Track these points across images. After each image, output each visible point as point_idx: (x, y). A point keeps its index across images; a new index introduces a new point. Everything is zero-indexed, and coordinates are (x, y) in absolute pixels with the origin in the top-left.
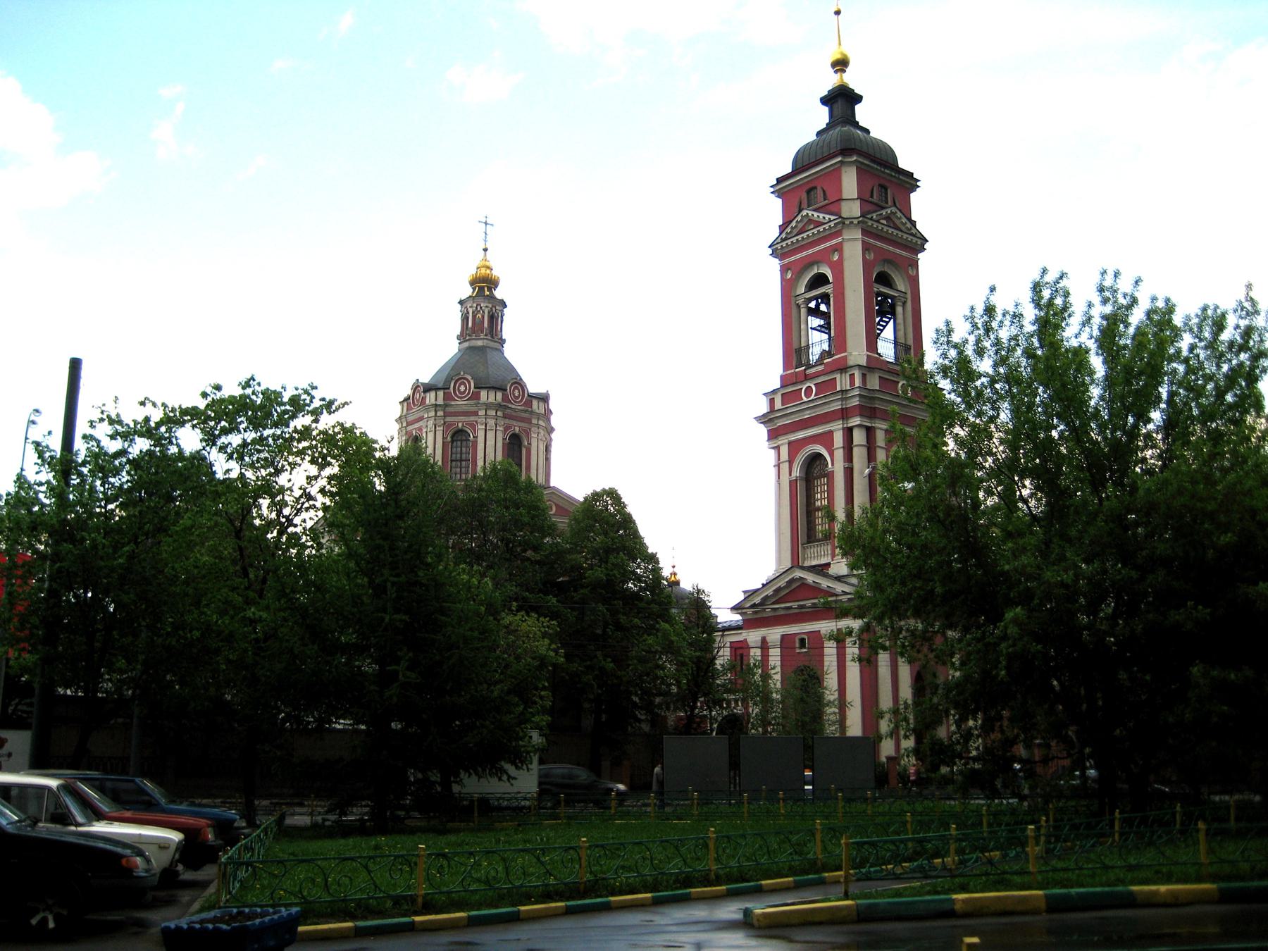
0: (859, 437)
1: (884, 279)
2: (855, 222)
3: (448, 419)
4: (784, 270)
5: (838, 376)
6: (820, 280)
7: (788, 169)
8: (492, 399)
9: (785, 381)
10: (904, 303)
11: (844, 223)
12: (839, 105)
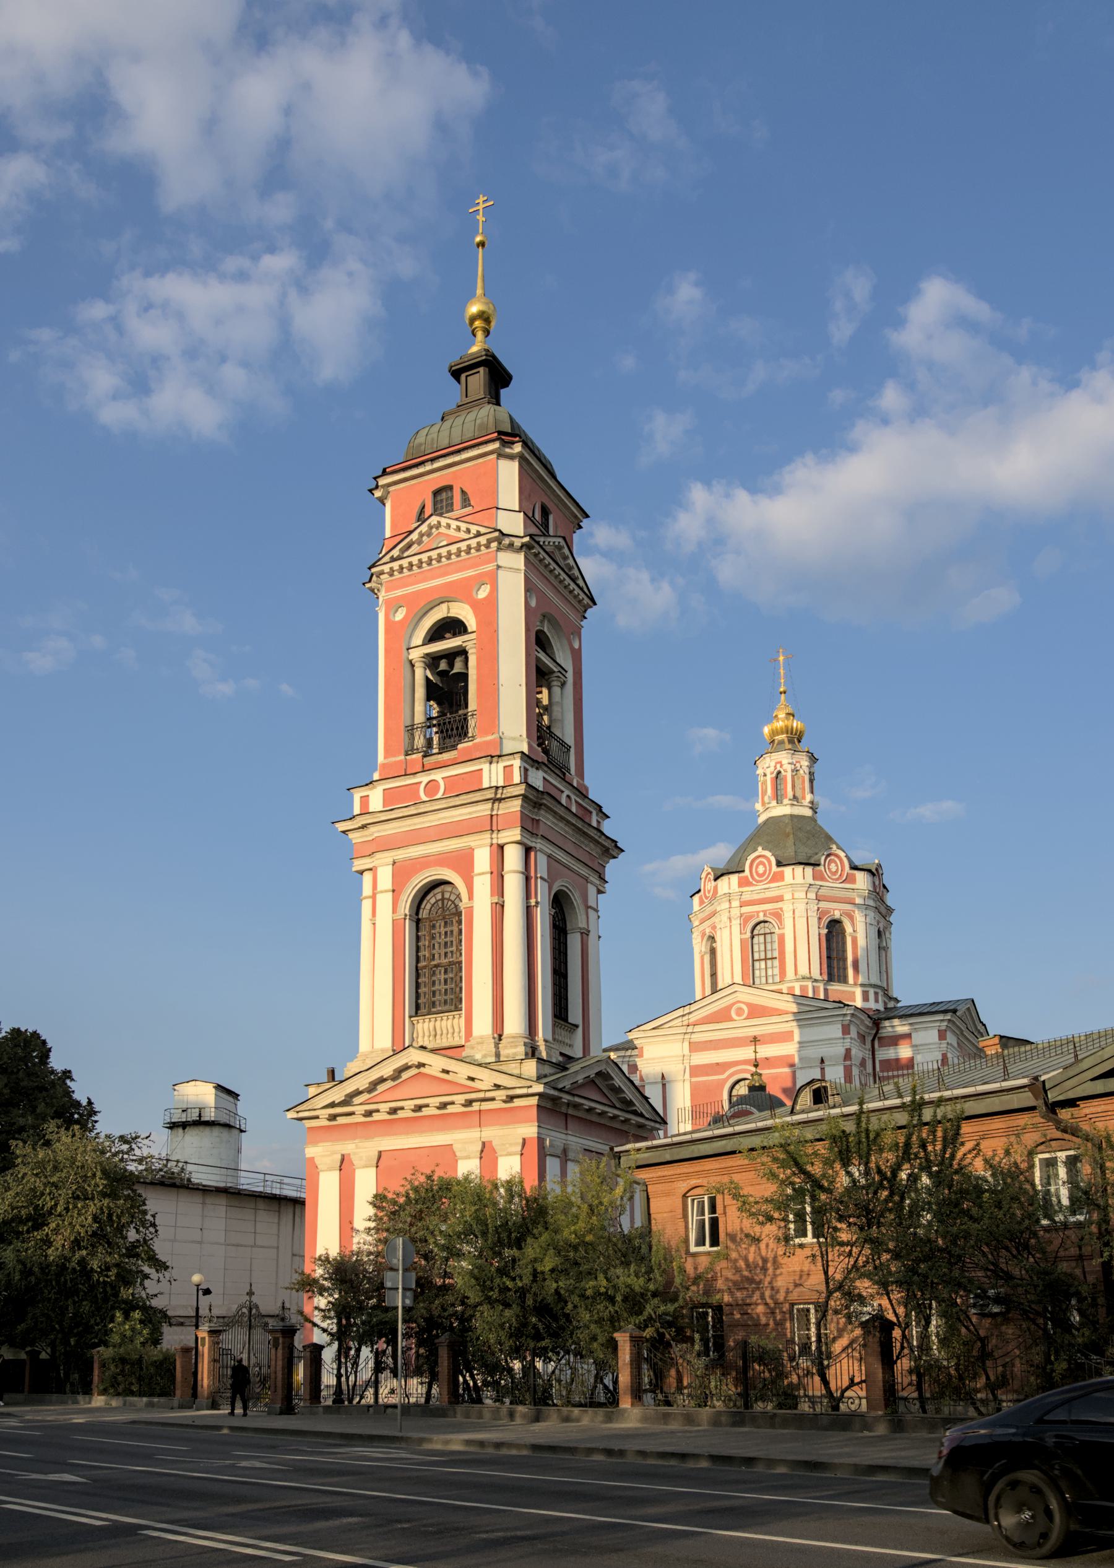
2: (518, 543)
3: (745, 909)
5: (485, 767)
6: (452, 626)
10: (563, 684)
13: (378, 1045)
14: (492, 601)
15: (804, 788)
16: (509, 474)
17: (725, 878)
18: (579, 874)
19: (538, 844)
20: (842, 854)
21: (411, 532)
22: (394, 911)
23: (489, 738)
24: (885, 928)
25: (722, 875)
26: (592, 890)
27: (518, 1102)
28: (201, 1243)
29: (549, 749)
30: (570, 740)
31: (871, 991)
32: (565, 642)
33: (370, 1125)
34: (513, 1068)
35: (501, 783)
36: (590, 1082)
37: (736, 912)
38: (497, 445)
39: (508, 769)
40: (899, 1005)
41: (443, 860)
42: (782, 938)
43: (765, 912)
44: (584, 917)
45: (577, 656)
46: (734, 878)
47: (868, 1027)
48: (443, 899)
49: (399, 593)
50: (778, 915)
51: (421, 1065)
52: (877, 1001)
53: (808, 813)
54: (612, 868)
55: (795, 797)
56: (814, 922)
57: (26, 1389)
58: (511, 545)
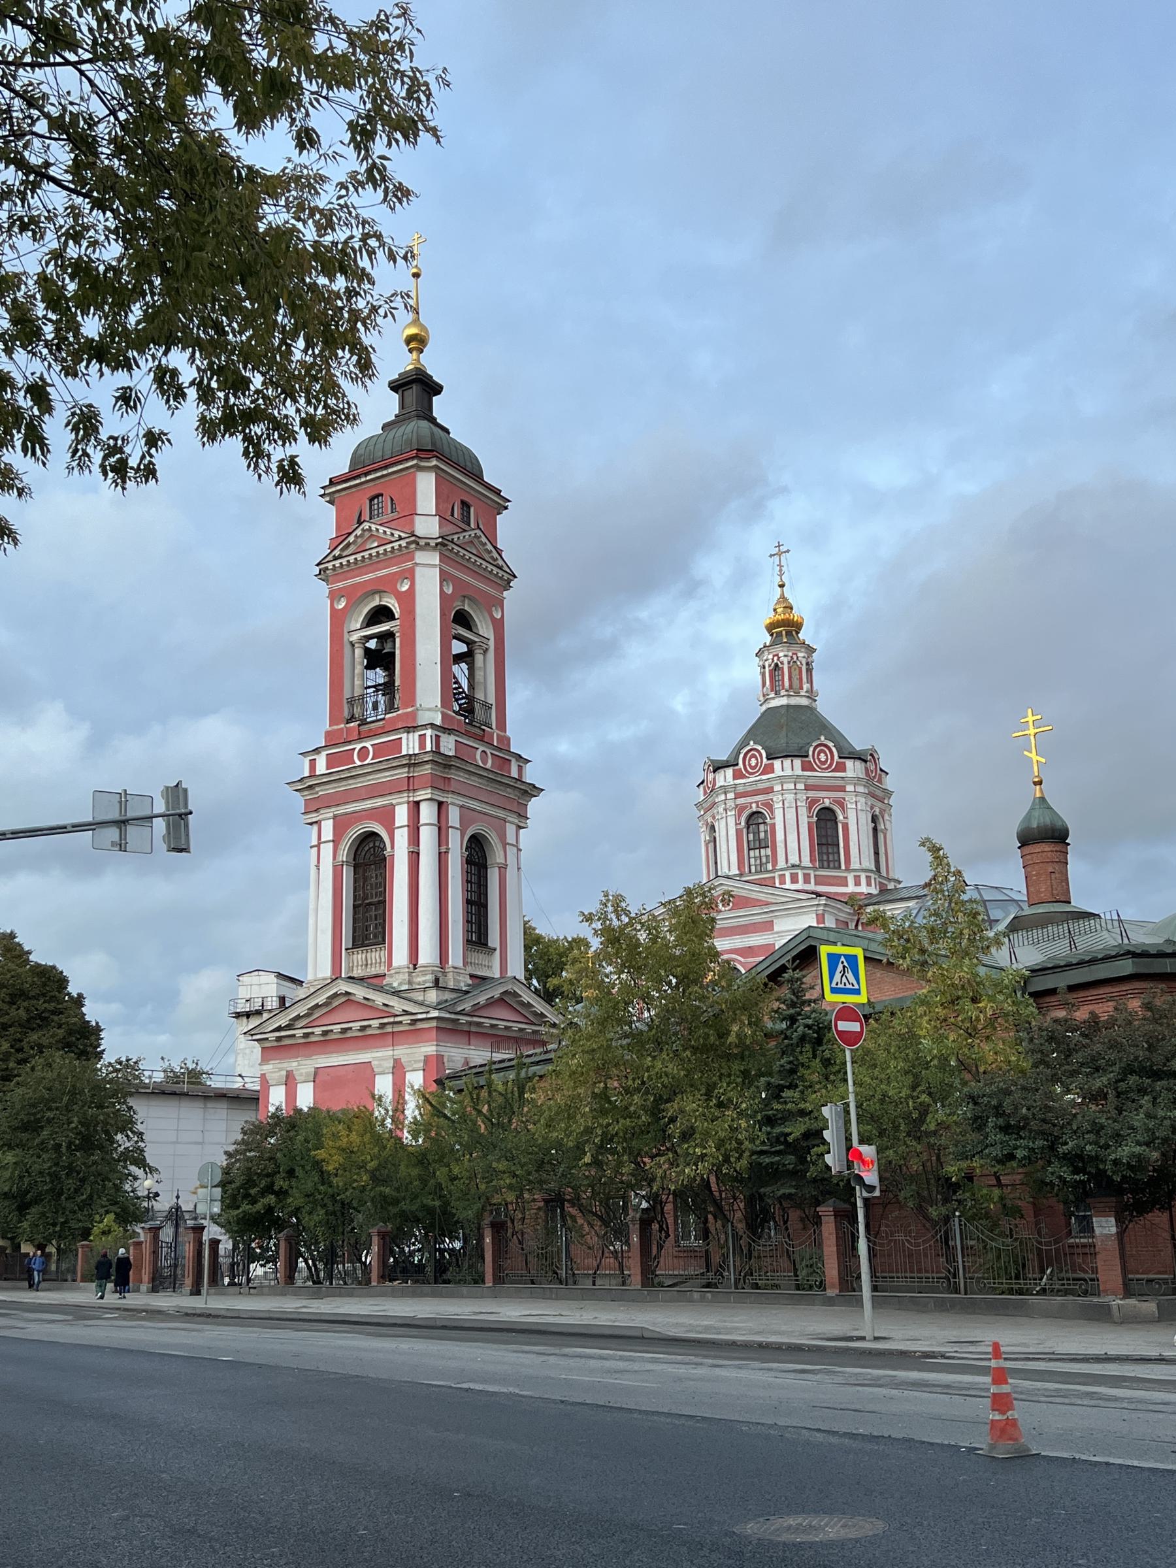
0: (427, 813)
1: (462, 619)
2: (433, 543)
3: (739, 801)
4: (334, 596)
5: (404, 736)
6: (381, 614)
7: (344, 468)
8: (788, 772)
9: (332, 740)
10: (486, 651)
11: (417, 543)
12: (413, 392)
13: (320, 976)
14: (410, 595)
15: (801, 679)
16: (426, 486)
17: (722, 771)
18: (496, 817)
19: (448, 798)
20: (831, 744)
21: (350, 534)
22: (334, 858)
23: (409, 710)
24: (882, 812)
25: (719, 768)
26: (510, 830)
27: (420, 1026)
28: (202, 1143)
29: (470, 712)
30: (492, 700)
31: (863, 876)
32: (486, 615)
33: (308, 1046)
34: (419, 996)
35: (417, 751)
36: (501, 1001)
37: (731, 804)
38: (415, 462)
39: (422, 738)
40: (901, 886)
41: (372, 814)
42: (773, 826)
43: (757, 802)
44: (502, 853)
45: (499, 626)
46: (729, 772)
47: (850, 914)
48: (374, 847)
49: (341, 584)
50: (769, 806)
51: (347, 993)
52: (869, 884)
53: (805, 702)
54: (534, 806)
55: (791, 686)
56: (803, 812)
57: (489, 1276)
58: (428, 544)
